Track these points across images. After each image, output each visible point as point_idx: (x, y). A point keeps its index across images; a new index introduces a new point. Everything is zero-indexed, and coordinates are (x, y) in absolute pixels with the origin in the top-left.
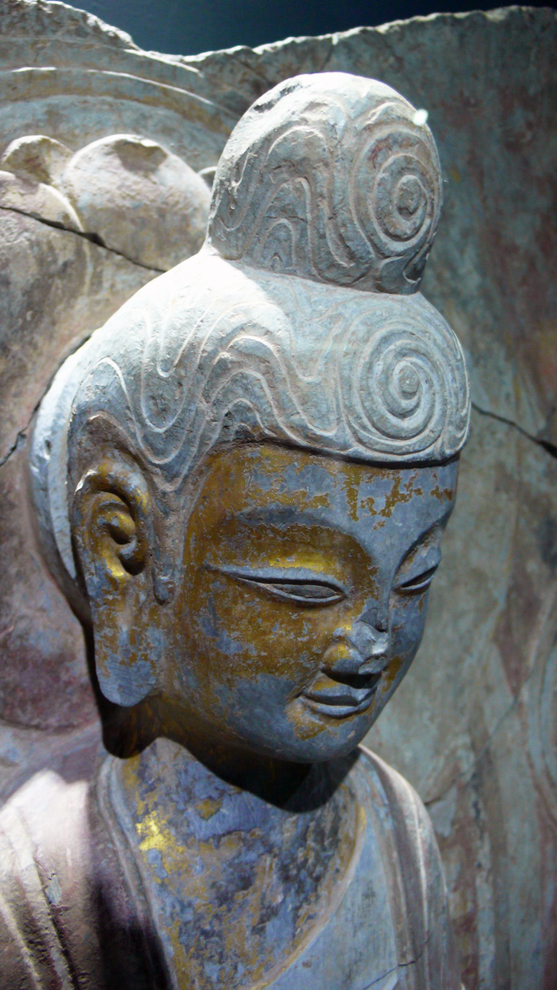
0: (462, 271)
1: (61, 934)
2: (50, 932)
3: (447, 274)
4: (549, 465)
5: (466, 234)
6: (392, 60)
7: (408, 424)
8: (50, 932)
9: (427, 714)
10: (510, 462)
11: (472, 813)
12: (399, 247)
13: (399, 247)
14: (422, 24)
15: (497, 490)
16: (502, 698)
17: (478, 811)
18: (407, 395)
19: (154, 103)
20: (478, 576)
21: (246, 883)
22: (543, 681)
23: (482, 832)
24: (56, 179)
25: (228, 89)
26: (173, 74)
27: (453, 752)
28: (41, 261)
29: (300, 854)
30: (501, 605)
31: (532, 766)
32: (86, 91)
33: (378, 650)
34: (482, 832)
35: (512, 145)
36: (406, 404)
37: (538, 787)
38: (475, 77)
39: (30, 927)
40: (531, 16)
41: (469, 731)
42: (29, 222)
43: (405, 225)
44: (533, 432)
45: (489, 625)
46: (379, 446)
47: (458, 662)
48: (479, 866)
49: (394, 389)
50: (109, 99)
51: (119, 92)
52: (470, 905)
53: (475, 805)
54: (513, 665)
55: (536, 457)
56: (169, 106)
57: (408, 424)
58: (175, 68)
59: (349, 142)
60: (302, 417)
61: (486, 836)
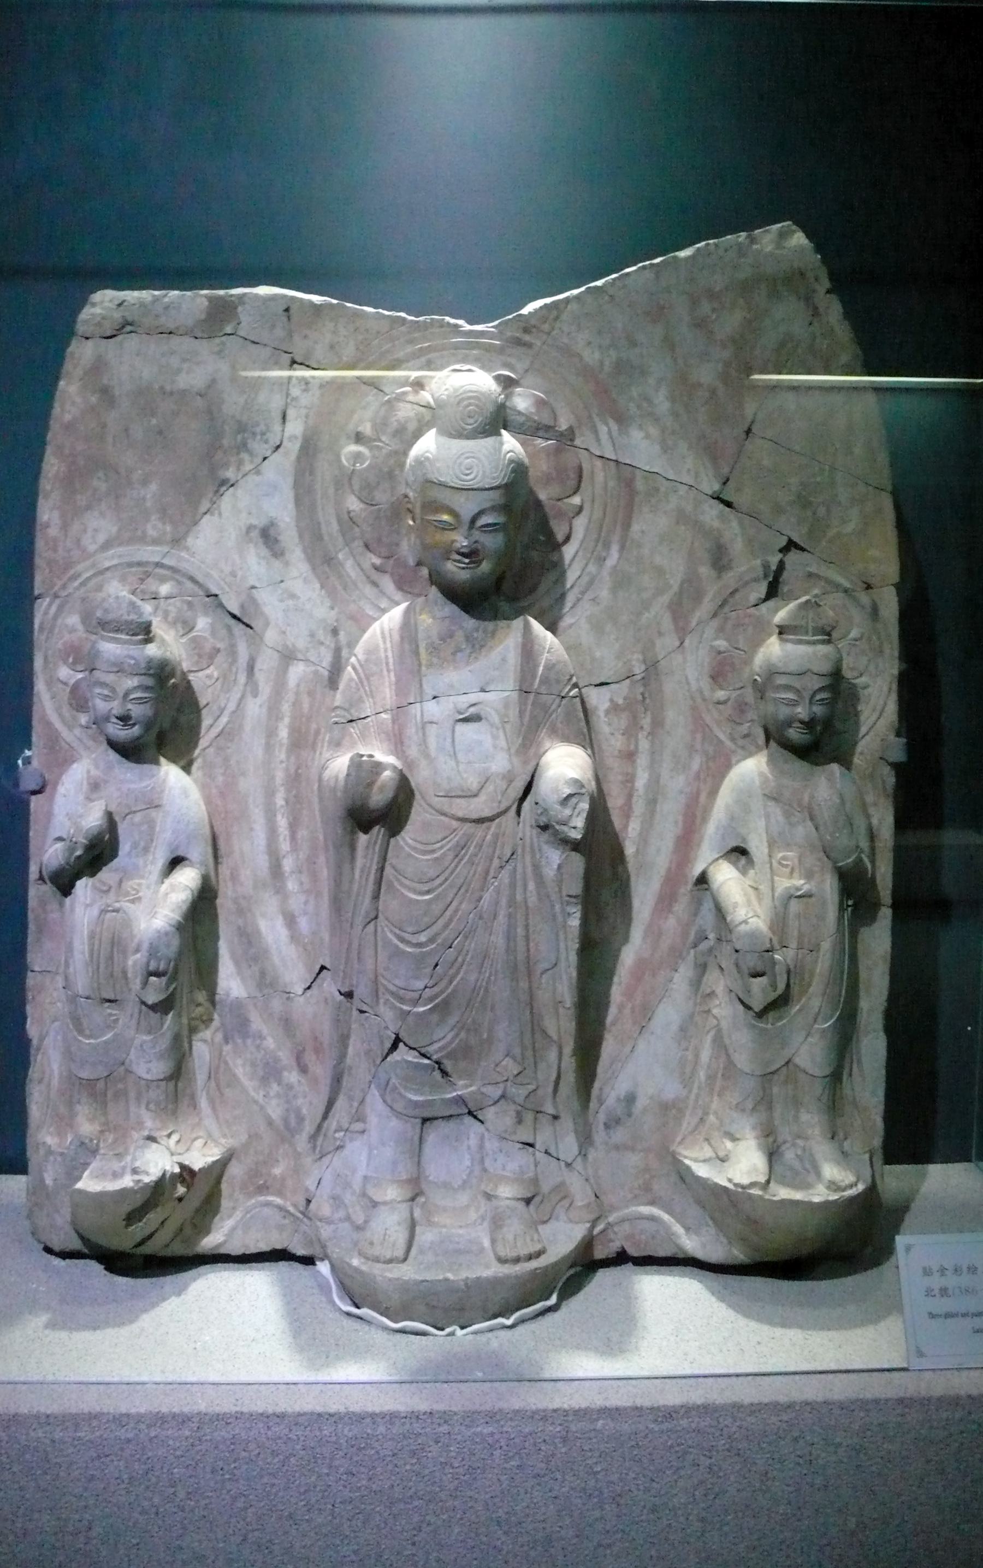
0: (656, 401)
1: (391, 636)
2: (387, 635)
3: (645, 405)
4: (721, 512)
5: (660, 381)
6: (607, 298)
7: (469, 478)
8: (387, 635)
9: (613, 637)
10: (689, 508)
11: (640, 698)
12: (470, 427)
13: (470, 427)
14: (628, 274)
15: (678, 523)
16: (671, 641)
17: (644, 698)
18: (468, 469)
19: (473, 348)
20: (660, 571)
21: (451, 636)
22: (701, 637)
23: (646, 710)
24: (427, 388)
25: (509, 334)
26: (482, 334)
27: (630, 660)
28: (419, 421)
29: (475, 635)
30: (676, 588)
31: (688, 683)
32: (444, 349)
33: (465, 544)
34: (646, 710)
35: (700, 324)
36: (468, 472)
37: (692, 698)
38: (670, 292)
39: (383, 633)
40: (716, 245)
41: (643, 653)
42: (416, 407)
43: (471, 421)
44: (710, 493)
45: (665, 599)
46: (459, 484)
47: (639, 614)
48: (642, 728)
49: (463, 468)
50: (452, 351)
51: (457, 347)
52: (632, 747)
53: (642, 694)
54: (681, 624)
55: (711, 507)
56: (479, 348)
57: (469, 478)
58: (483, 331)
59: (452, 400)
60: (437, 475)
61: (649, 713)
